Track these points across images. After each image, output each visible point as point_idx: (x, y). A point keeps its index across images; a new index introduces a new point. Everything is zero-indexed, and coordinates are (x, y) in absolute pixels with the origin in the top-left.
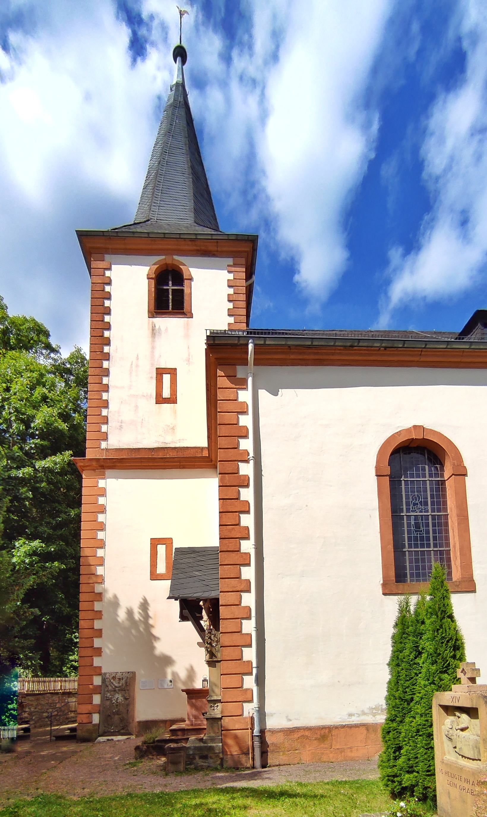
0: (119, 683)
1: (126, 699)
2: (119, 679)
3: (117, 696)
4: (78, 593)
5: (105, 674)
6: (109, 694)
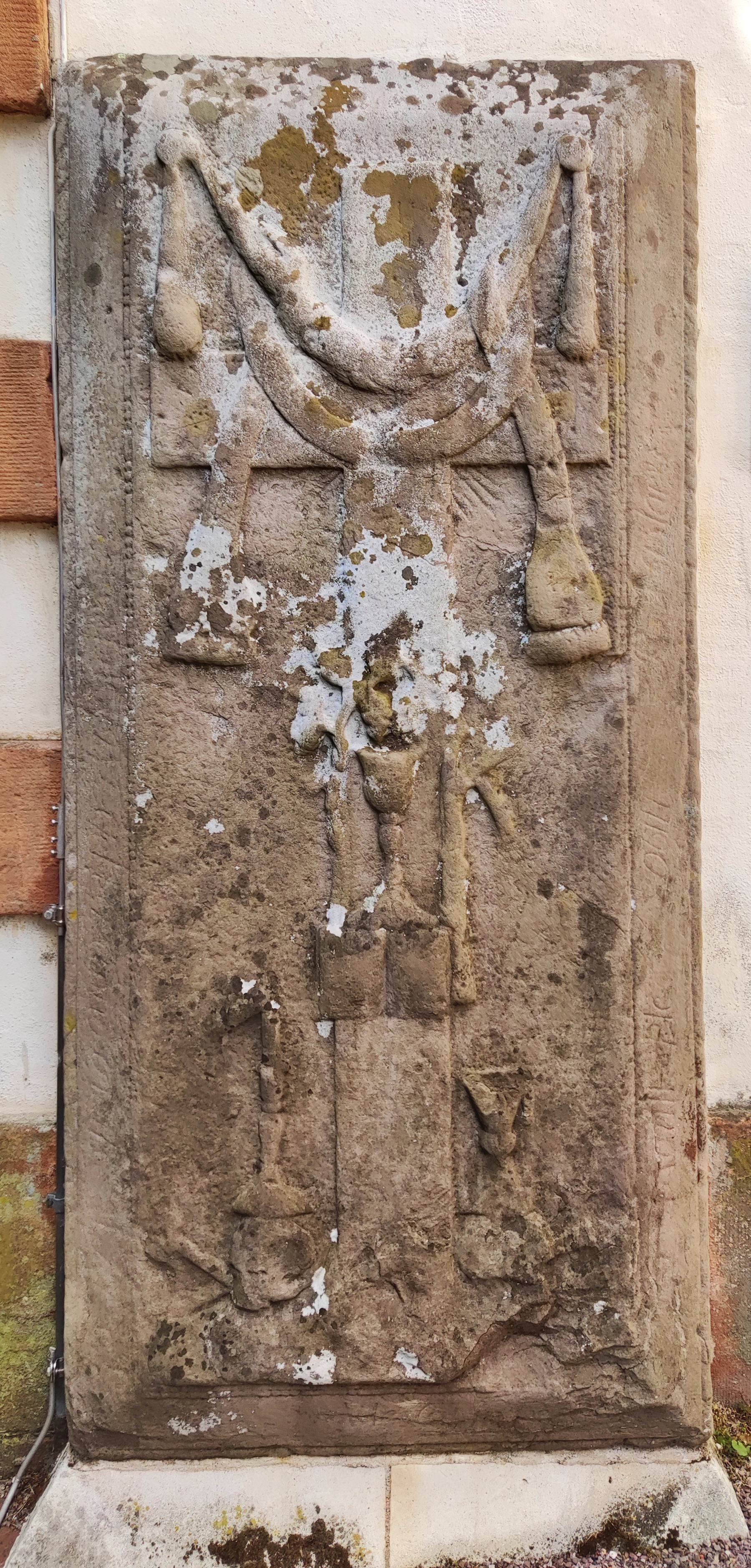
0: (403, 287)
1: (553, 663)
2: (411, 201)
3: (375, 587)
4: (60, 1452)
5: (124, 80)
6: (212, 543)
